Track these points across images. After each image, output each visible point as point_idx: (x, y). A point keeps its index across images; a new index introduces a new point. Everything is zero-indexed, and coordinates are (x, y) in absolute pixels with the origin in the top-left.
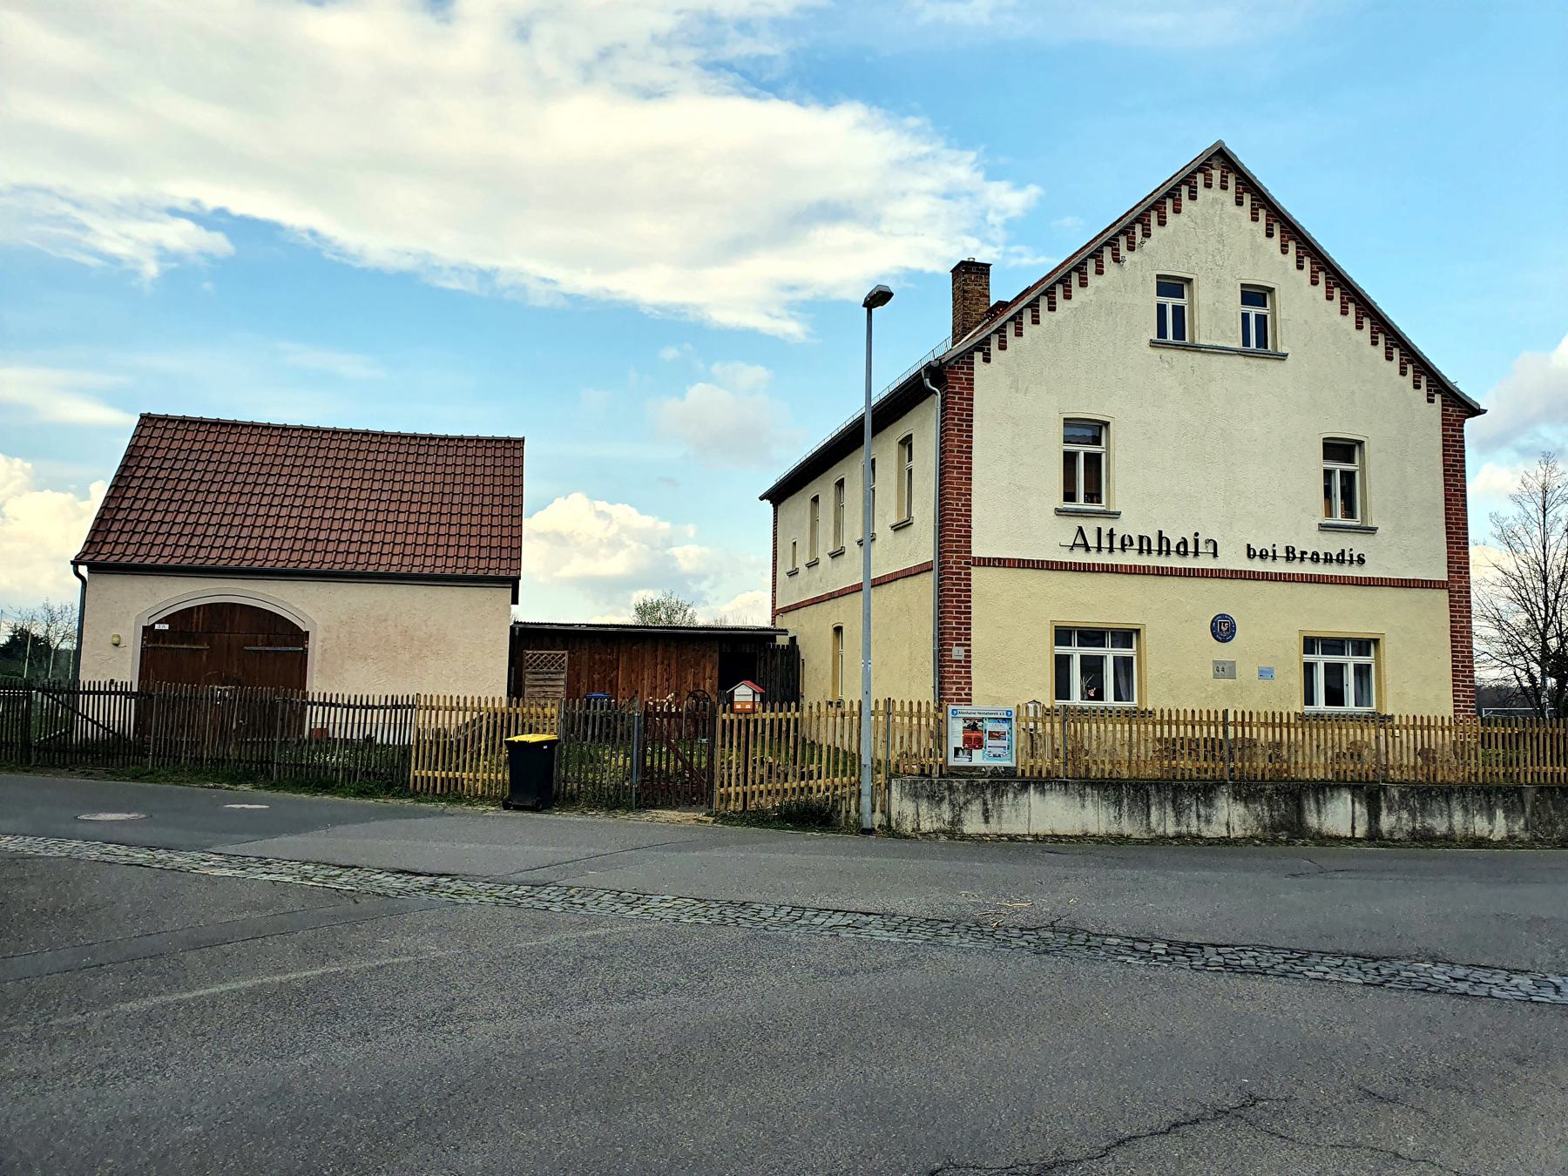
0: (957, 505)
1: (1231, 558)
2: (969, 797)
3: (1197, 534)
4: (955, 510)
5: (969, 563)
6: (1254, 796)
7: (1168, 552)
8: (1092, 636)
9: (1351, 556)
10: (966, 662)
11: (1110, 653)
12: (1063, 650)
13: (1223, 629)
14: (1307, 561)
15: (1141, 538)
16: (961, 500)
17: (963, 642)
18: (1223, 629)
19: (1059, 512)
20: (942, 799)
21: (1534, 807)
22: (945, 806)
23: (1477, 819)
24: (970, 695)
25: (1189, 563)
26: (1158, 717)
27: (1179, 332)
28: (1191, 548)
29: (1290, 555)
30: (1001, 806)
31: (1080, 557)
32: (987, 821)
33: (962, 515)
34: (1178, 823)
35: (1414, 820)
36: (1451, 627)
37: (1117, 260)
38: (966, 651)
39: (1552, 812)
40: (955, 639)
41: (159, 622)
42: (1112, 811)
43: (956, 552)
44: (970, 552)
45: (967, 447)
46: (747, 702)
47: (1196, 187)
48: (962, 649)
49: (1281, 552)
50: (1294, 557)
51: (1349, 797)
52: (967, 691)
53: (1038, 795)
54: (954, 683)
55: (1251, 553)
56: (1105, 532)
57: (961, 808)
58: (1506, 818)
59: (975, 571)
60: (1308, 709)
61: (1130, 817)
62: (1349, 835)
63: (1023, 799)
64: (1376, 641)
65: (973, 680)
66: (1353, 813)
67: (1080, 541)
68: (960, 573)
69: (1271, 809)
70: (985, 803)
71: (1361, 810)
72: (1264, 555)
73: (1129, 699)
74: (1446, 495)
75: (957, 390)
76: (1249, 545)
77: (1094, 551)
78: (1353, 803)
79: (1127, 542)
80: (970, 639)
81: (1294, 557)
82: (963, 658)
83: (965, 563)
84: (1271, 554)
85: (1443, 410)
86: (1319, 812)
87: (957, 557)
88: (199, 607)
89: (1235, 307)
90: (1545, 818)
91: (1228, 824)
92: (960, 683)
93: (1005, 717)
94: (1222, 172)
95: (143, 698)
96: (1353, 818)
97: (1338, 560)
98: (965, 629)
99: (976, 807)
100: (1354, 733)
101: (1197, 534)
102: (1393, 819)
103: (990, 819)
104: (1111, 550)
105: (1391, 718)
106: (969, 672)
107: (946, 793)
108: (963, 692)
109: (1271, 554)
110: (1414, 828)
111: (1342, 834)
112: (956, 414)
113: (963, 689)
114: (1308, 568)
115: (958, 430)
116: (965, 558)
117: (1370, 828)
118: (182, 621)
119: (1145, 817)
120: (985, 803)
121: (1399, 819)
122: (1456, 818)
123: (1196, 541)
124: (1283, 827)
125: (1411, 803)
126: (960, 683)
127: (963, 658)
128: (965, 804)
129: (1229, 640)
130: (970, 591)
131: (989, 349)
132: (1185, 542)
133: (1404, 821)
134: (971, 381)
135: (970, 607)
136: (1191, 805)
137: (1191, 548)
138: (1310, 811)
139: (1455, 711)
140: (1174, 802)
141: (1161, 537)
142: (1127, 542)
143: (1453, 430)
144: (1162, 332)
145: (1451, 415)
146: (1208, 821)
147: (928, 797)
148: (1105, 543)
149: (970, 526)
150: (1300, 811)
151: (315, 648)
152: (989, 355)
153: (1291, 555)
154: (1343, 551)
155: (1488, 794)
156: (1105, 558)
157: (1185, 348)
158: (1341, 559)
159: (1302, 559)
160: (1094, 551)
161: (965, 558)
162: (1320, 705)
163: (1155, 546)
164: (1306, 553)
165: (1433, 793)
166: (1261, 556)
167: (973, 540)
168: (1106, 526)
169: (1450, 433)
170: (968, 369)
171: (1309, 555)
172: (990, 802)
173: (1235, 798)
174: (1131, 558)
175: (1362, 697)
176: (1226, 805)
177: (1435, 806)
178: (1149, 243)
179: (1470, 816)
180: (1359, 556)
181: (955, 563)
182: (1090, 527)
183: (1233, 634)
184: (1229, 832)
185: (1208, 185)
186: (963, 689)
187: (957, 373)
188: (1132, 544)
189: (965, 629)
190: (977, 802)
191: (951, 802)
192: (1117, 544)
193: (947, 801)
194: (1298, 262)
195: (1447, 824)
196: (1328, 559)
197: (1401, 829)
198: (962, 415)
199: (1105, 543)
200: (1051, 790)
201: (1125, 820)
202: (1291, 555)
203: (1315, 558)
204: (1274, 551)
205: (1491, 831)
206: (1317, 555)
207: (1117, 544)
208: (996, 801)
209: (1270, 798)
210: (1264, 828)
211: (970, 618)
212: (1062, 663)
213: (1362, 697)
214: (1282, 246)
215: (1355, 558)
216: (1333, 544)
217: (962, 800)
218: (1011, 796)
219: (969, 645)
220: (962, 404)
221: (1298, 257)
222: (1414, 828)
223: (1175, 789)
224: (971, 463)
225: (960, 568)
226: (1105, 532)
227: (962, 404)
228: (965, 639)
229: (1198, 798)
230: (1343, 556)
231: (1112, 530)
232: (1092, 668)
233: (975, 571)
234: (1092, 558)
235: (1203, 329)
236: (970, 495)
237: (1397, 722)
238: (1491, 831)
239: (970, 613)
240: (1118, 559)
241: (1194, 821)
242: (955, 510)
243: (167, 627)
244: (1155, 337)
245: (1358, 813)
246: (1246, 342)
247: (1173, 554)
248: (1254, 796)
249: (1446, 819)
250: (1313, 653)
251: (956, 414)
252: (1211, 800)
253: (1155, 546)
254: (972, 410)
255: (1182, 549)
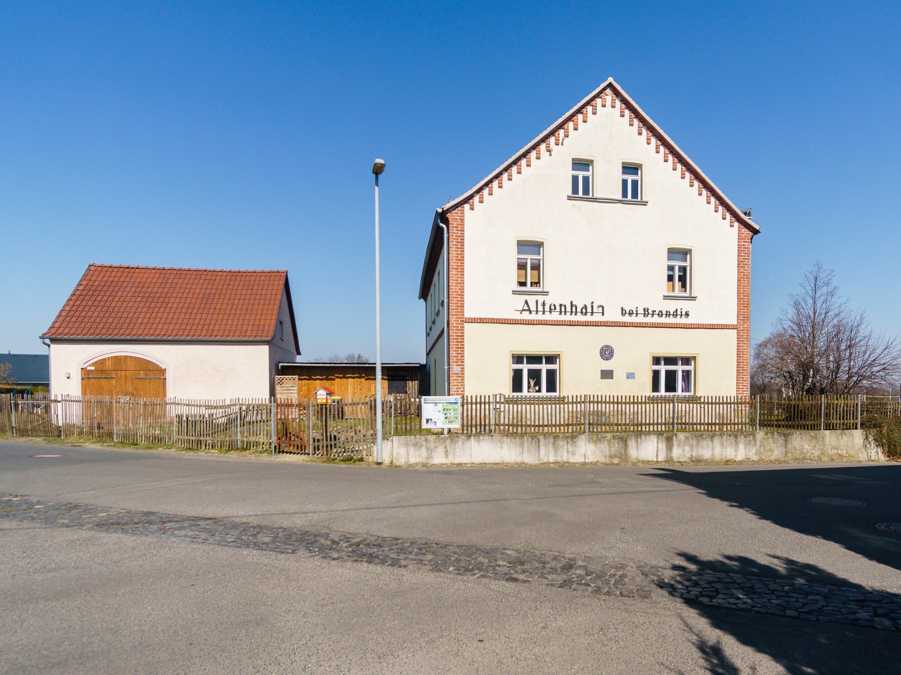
0: (456, 289)
1: (613, 315)
2: (437, 444)
3: (592, 303)
4: (455, 292)
5: (463, 321)
6: (600, 440)
7: (576, 312)
8: (535, 359)
9: (681, 312)
10: (461, 374)
11: (544, 367)
12: (656, 367)
13: (607, 353)
14: (656, 316)
15: (561, 305)
16: (458, 286)
17: (460, 363)
18: (607, 353)
19: (514, 292)
20: (421, 446)
21: (761, 442)
22: (423, 450)
23: (729, 449)
24: (464, 391)
25: (589, 318)
26: (702, 401)
27: (586, 191)
28: (589, 310)
29: (646, 312)
30: (455, 448)
31: (526, 316)
32: (447, 456)
33: (459, 295)
34: (556, 455)
35: (692, 451)
36: (738, 349)
37: (549, 151)
38: (461, 368)
39: (772, 445)
40: (456, 362)
41: (89, 366)
42: (518, 450)
43: (455, 315)
44: (463, 315)
45: (461, 257)
46: (324, 399)
47: (596, 107)
48: (459, 367)
49: (641, 311)
50: (648, 314)
51: (656, 440)
52: (462, 389)
53: (476, 443)
54: (455, 385)
55: (623, 311)
56: (540, 303)
57: (432, 450)
58: (745, 448)
59: (733, 321)
60: (656, 394)
61: (528, 452)
62: (655, 460)
63: (468, 444)
64: (694, 358)
65: (466, 384)
66: (658, 448)
67: (526, 308)
68: (458, 327)
69: (610, 447)
70: (446, 447)
71: (662, 446)
72: (631, 314)
73: (555, 391)
74: (738, 278)
75: (455, 225)
76: (622, 308)
77: (534, 313)
78: (658, 443)
79: (553, 307)
80: (464, 362)
81: (648, 314)
82: (460, 372)
83: (461, 321)
84: (635, 312)
85: (739, 231)
86: (637, 448)
87: (456, 318)
88: (109, 358)
89: (619, 176)
90: (768, 448)
91: (585, 455)
92: (458, 385)
93: (455, 402)
94: (612, 97)
95: (87, 404)
96: (657, 451)
97: (673, 315)
98: (461, 357)
99: (441, 449)
100: (682, 407)
101: (592, 303)
102: (680, 450)
103: (449, 456)
104: (544, 312)
105: (700, 398)
106: (463, 380)
107: (424, 443)
108: (460, 390)
109: (635, 312)
110: (692, 455)
111: (650, 459)
112: (454, 239)
113: (460, 388)
114: (656, 319)
115: (456, 248)
116: (460, 318)
117: (667, 455)
118: (100, 365)
119: (537, 453)
120: (446, 447)
121: (684, 450)
122: (716, 449)
123: (592, 306)
124: (616, 456)
125: (691, 442)
126: (458, 385)
127: (460, 372)
128: (435, 448)
129: (610, 359)
130: (463, 336)
131: (473, 202)
132: (586, 307)
133: (686, 452)
134: (462, 220)
135: (464, 345)
136: (563, 445)
137: (589, 310)
138: (632, 447)
139: (737, 394)
140: (554, 444)
141: (572, 306)
142: (553, 307)
143: (744, 242)
144: (575, 190)
145: (743, 234)
146: (573, 454)
147: (414, 445)
148: (540, 308)
149: (463, 301)
150: (626, 446)
151: (169, 376)
152: (473, 205)
153: (646, 313)
154: (677, 310)
155: (736, 436)
156: (540, 317)
157: (588, 200)
158: (675, 315)
159: (653, 315)
160: (534, 313)
161: (460, 318)
162: (662, 392)
163: (568, 309)
164: (655, 311)
165: (704, 437)
166: (630, 314)
167: (465, 308)
168: (541, 299)
169: (743, 243)
170: (461, 213)
171: (657, 312)
172: (448, 447)
173: (589, 441)
174: (555, 316)
175: (687, 388)
176: (584, 445)
177: (705, 443)
178: (566, 140)
179: (725, 448)
180: (686, 313)
181: (454, 321)
182: (532, 300)
183: (612, 356)
184: (585, 459)
185: (604, 106)
186: (460, 388)
187: (454, 216)
188: (555, 309)
189: (461, 357)
190: (441, 447)
191: (426, 448)
192: (547, 309)
193: (424, 447)
194: (657, 148)
195: (711, 453)
196: (668, 314)
197: (684, 456)
198: (458, 239)
199: (540, 308)
200: (483, 439)
201: (525, 455)
202: (646, 313)
203: (660, 314)
204: (637, 311)
205: (736, 456)
206: (662, 312)
207: (547, 309)
208: (452, 446)
209: (609, 441)
210: (605, 457)
211: (464, 351)
212: (656, 374)
213: (687, 388)
214: (647, 139)
215: (684, 313)
216: (671, 306)
217: (432, 446)
218: (460, 443)
219: (463, 365)
220: (458, 233)
221: (657, 145)
222: (692, 455)
223: (554, 437)
224: (463, 266)
225: (458, 324)
226: (540, 303)
227: (458, 233)
228: (461, 362)
229: (568, 442)
230: (677, 312)
231: (544, 301)
232: (671, 377)
233: (733, 321)
234: (534, 317)
235: (599, 189)
236: (463, 283)
237: (702, 401)
238: (736, 456)
239: (463, 348)
240: (548, 317)
241: (565, 454)
242: (455, 292)
243: (93, 368)
244: (570, 194)
245: (660, 448)
246: (625, 194)
247: (579, 314)
248: (600, 440)
249: (710, 450)
250: (375, 367)
251: (454, 239)
252: (575, 443)
253: (568, 309)
254: (463, 237)
255: (584, 310)
